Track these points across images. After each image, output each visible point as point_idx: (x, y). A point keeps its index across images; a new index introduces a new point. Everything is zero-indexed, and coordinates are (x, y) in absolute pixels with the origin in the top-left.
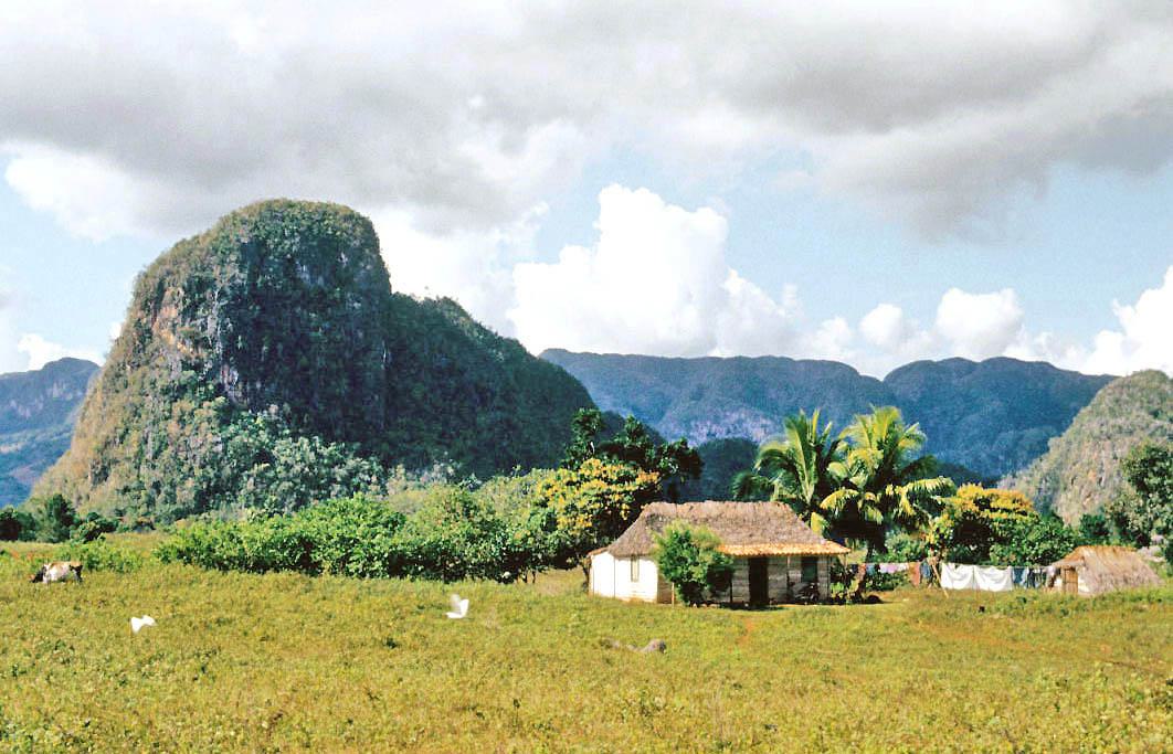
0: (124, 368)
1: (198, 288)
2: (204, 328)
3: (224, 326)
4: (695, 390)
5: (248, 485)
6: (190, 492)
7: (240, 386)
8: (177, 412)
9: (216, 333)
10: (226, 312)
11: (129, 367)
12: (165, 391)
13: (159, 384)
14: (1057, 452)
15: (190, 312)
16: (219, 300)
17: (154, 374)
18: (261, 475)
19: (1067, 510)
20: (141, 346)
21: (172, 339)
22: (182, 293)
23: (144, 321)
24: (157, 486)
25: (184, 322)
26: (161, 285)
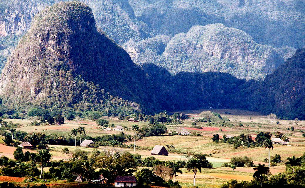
0: (36, 58)
1: (60, 36)
2: (63, 48)
3: (69, 48)
4: (52, 107)
5: (84, 96)
6: (71, 98)
7: (74, 65)
8: (60, 74)
9: (67, 50)
10: (70, 43)
11: (38, 58)
12: (55, 67)
13: (53, 65)
14: (4, 84)
15: (58, 43)
16: (67, 40)
17: (50, 61)
18: (87, 93)
19: (283, 100)
20: (42, 52)
21: (52, 50)
22: (56, 37)
23: (42, 44)
24: (60, 96)
25: (56, 46)
26: (48, 34)
